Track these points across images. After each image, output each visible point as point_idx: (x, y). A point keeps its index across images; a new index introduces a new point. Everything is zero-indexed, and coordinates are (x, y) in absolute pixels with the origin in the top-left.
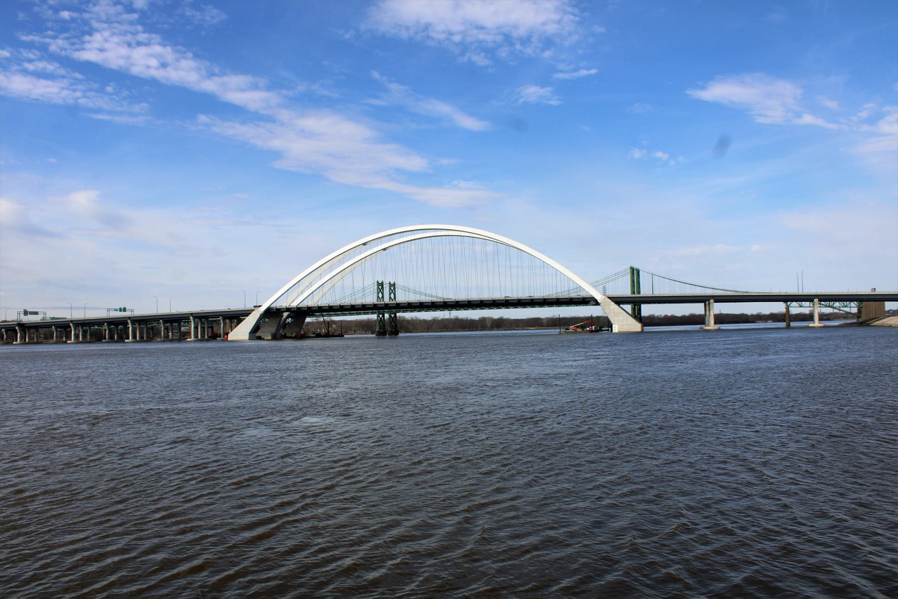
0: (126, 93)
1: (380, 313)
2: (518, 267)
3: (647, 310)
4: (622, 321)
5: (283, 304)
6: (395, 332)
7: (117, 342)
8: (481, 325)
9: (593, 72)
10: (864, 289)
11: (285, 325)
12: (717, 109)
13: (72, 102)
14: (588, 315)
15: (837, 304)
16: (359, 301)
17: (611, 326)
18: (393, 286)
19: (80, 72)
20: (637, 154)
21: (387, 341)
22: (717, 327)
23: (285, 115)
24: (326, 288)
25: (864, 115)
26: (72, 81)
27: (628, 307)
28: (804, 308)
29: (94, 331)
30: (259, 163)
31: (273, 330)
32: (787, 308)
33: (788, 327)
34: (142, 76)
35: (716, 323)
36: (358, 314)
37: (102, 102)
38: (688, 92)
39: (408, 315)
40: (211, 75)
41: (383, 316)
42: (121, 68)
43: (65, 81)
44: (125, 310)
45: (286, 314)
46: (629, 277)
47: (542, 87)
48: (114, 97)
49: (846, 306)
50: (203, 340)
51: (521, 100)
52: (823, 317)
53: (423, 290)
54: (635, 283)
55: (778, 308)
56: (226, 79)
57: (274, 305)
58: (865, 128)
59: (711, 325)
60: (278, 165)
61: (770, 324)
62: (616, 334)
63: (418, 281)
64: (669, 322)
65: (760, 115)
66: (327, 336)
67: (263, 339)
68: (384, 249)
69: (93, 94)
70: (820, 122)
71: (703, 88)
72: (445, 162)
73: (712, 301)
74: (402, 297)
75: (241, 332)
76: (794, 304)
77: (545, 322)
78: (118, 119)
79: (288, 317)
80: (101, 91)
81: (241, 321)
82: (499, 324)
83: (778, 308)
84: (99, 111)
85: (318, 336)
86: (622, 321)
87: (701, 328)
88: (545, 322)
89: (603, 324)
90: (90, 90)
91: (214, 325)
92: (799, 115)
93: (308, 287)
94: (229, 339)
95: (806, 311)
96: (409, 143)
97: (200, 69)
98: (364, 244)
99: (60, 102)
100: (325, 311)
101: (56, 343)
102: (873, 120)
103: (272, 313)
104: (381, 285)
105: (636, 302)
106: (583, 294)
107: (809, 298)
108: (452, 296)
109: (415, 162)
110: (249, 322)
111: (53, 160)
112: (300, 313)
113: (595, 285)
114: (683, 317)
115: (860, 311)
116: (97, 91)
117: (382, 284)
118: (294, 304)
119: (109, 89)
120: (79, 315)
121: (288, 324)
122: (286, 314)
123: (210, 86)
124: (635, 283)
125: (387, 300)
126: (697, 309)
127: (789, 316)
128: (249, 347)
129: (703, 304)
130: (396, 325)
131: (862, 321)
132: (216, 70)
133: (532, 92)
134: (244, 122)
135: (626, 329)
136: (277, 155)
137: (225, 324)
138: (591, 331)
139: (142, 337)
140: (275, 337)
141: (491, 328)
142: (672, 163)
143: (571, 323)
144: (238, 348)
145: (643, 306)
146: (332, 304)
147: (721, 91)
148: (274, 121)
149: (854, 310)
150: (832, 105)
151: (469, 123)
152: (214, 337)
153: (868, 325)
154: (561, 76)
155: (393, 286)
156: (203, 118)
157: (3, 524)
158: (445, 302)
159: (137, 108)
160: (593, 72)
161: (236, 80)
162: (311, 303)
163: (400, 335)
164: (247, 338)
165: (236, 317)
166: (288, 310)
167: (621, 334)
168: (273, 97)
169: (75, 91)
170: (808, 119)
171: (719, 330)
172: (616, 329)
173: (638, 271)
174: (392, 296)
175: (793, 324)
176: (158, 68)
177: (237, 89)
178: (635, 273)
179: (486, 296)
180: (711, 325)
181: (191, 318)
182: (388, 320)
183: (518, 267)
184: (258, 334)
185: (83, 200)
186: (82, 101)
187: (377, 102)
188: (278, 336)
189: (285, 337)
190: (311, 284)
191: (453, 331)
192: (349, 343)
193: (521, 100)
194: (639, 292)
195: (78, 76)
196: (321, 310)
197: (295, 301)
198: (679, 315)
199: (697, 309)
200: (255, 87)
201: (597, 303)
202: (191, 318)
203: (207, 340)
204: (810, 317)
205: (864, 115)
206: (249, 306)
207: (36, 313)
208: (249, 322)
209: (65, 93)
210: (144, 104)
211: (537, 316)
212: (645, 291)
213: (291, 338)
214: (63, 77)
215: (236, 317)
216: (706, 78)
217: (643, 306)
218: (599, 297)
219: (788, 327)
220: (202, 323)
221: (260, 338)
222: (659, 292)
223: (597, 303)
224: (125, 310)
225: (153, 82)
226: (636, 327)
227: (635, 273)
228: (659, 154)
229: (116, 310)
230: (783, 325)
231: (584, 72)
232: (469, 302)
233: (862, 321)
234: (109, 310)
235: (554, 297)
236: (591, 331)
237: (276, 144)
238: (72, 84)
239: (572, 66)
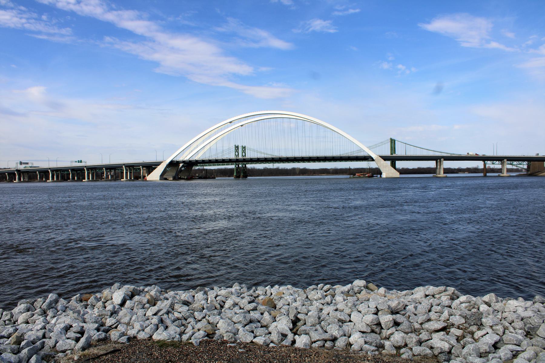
0: (54, 21)
2: (309, 137)
3: (400, 164)
4: (388, 171)
5: (181, 159)
6: (245, 176)
7: (76, 181)
8: (293, 172)
9: (358, 11)
10: (532, 154)
11: (181, 171)
12: (436, 35)
13: (20, 26)
15: (515, 163)
16: (226, 157)
18: (244, 148)
19: (24, 6)
20: (385, 66)
21: (241, 181)
22: (445, 175)
23: (162, 37)
24: (206, 149)
25: (530, 42)
26: (19, 11)
27: (389, 163)
28: (497, 165)
29: (62, 174)
30: (147, 70)
31: (174, 174)
32: (485, 165)
33: (485, 176)
34: (65, 9)
35: (444, 173)
36: (213, 165)
37: (40, 27)
38: (419, 25)
39: (249, 166)
40: (111, 9)
41: (238, 165)
42: (50, 3)
43: (14, 11)
44: (81, 162)
45: (181, 165)
46: (389, 144)
47: (325, 21)
48: (48, 23)
49: (520, 164)
50: (58, 180)
51: (311, 29)
52: (509, 170)
53: (263, 151)
54: (393, 149)
55: (480, 164)
56: (120, 12)
57: (175, 159)
58: (531, 51)
59: (442, 174)
60: (157, 71)
61: (467, 174)
63: (261, 145)
64: (429, 172)
65: (464, 42)
69: (33, 21)
70: (502, 47)
71: (429, 23)
72: (264, 69)
73: (442, 159)
74: (250, 155)
75: (155, 176)
76: (489, 162)
77: (331, 171)
78: (56, 39)
79: (183, 166)
80: (39, 20)
82: (304, 172)
83: (480, 164)
84: (39, 33)
86: (388, 171)
87: (434, 176)
88: (331, 171)
89: (378, 172)
90: (31, 18)
91: (138, 171)
92: (488, 42)
93: (195, 148)
95: (499, 166)
96: (244, 56)
97: (102, 5)
98: (230, 122)
99: (12, 26)
101: (40, 182)
102: (536, 46)
103: (173, 164)
104: (237, 147)
105: (393, 160)
106: (366, 155)
107: (500, 159)
108: (277, 154)
109: (245, 69)
110: (159, 170)
111: (14, 66)
112: (189, 164)
113: (370, 148)
114: (413, 169)
115: (529, 167)
116: (35, 19)
117: (238, 147)
119: (44, 17)
120: (54, 165)
121: (184, 171)
122: (181, 165)
123: (111, 17)
124: (393, 149)
125: (240, 157)
126: (432, 164)
127: (487, 170)
128: (160, 184)
129: (435, 162)
131: (531, 173)
132: (114, 6)
133: (318, 24)
134: (134, 42)
135: (390, 175)
136: (156, 64)
137: (126, 169)
138: (369, 177)
139: (131, 178)
140: (175, 179)
141: (299, 175)
142: (408, 72)
144: (154, 185)
147: (441, 25)
148: (154, 41)
149: (526, 167)
150: (510, 35)
151: (278, 44)
152: (137, 178)
153: (536, 176)
154: (336, 13)
155: (244, 148)
156: (108, 39)
158: (280, 158)
159: (64, 31)
160: (358, 11)
161: (127, 14)
162: (197, 158)
165: (150, 167)
166: (184, 162)
167: (387, 178)
168: (153, 26)
169: (21, 18)
170: (494, 45)
171: (446, 177)
172: (384, 175)
173: (395, 141)
174: (244, 154)
175: (488, 174)
176: (75, 4)
177: (129, 21)
178: (393, 142)
180: (505, 174)
181: (124, 166)
182: (240, 169)
183: (309, 137)
184: (165, 177)
185: (36, 92)
186: (27, 26)
187: (220, 29)
189: (181, 179)
190: (197, 147)
191: (261, 176)
192: (219, 182)
193: (311, 29)
195: (23, 8)
196: (204, 162)
197: (186, 157)
199: (432, 164)
200: (140, 18)
201: (373, 160)
202: (124, 166)
203: (133, 180)
204: (500, 171)
205: (530, 42)
207: (27, 163)
208: (159, 170)
209: (15, 20)
210: (68, 29)
212: (399, 152)
213: (184, 179)
214: (12, 9)
215: (150, 167)
216: (430, 17)
218: (374, 156)
219: (485, 176)
220: (130, 169)
221: (166, 179)
223: (373, 160)
224: (81, 162)
225: (72, 13)
226: (397, 175)
227: (393, 142)
228: (400, 66)
229: (76, 162)
230: (482, 174)
231: (352, 11)
232: (295, 158)
233: (531, 173)
234: (72, 162)
236: (369, 177)
237: (156, 57)
238: (19, 14)
239: (344, 7)
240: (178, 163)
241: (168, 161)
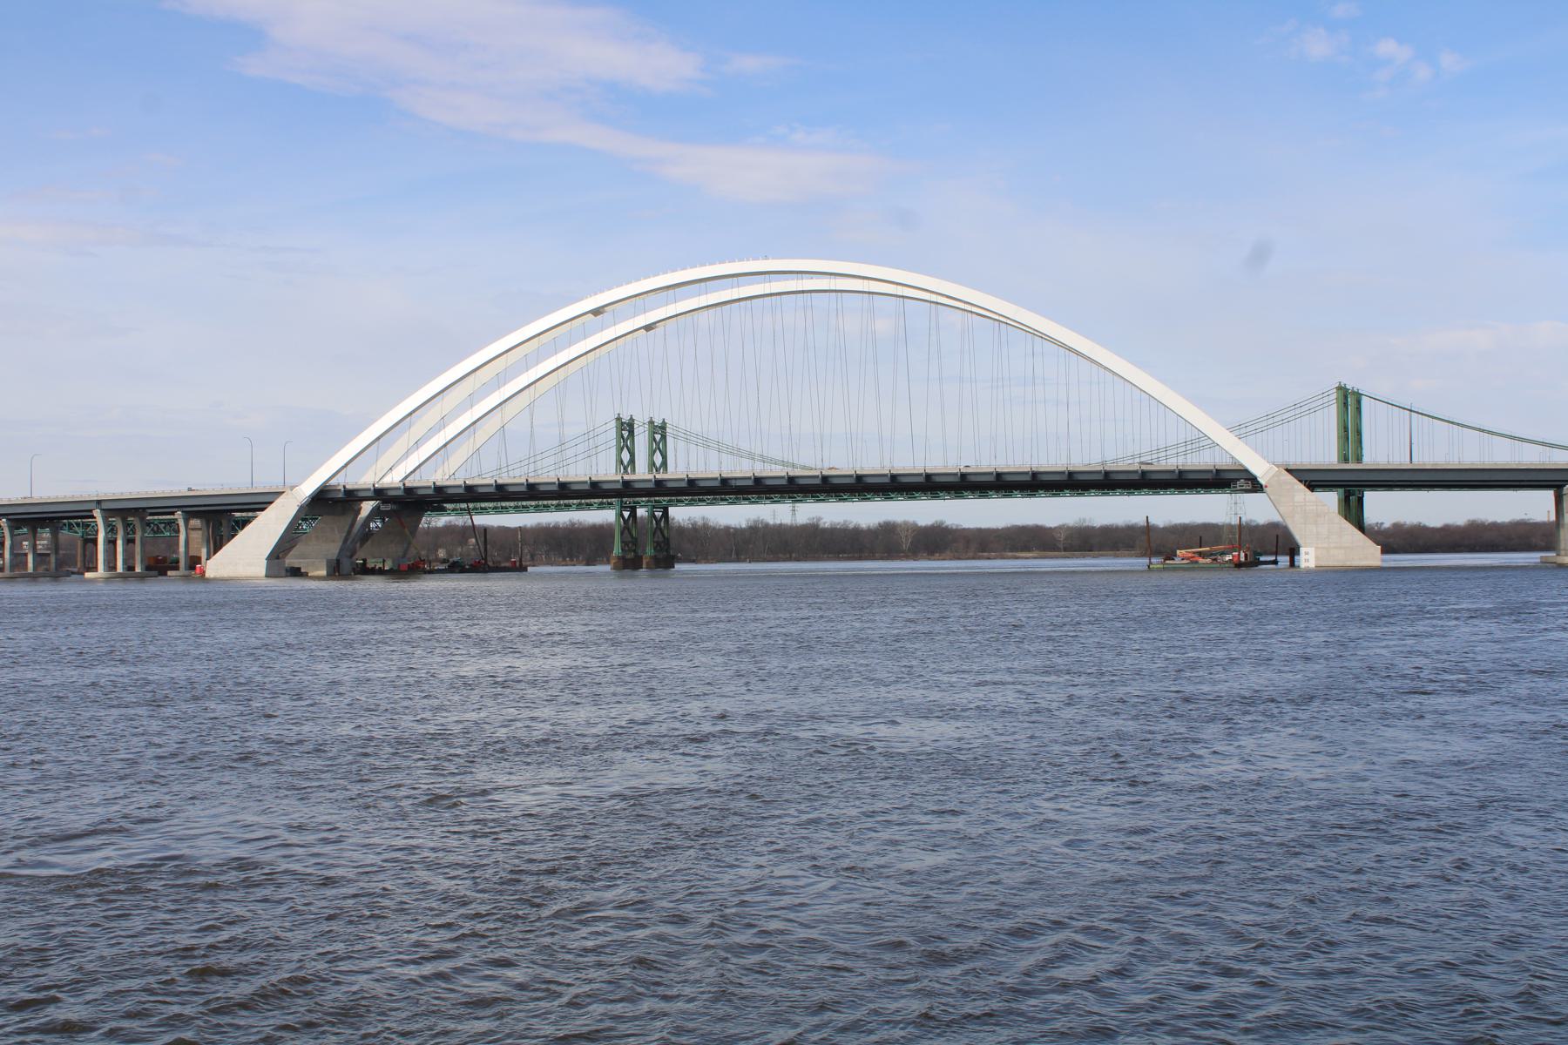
1: (623, 507)
3: (1382, 507)
4: (1325, 538)
5: (364, 478)
6: (665, 560)
8: (884, 543)
14: (1138, 519)
16: (578, 472)
17: (1293, 551)
18: (659, 432)
21: (643, 583)
24: (482, 434)
27: (1331, 499)
31: (333, 550)
45: (367, 507)
46: (1333, 411)
53: (745, 446)
57: (333, 482)
62: (1308, 571)
66: (480, 567)
67: (304, 575)
68: (648, 328)
74: (683, 464)
75: (244, 557)
79: (375, 513)
81: (244, 523)
82: (935, 541)
85: (455, 568)
86: (1325, 538)
87: (1544, 561)
91: (165, 535)
94: (209, 574)
98: (597, 312)
100: (486, 497)
103: (329, 503)
104: (626, 429)
105: (1350, 486)
106: (1222, 462)
109: (661, 64)
110: (266, 529)
112: (408, 504)
113: (1240, 430)
114: (1447, 530)
117: (663, 427)
118: (394, 479)
121: (383, 533)
122: (367, 507)
125: (642, 472)
129: (1549, 495)
130: (667, 541)
137: (111, 529)
143: (1177, 542)
144: (237, 601)
145: (1370, 498)
146: (504, 479)
152: (159, 566)
157: (1565, 924)
162: (448, 474)
163: (678, 566)
164: (263, 572)
165: (223, 518)
166: (379, 494)
172: (1308, 558)
173: (1358, 397)
174: (658, 459)
178: (1349, 401)
179: (873, 463)
181: (97, 513)
182: (641, 526)
188: (346, 565)
189: (365, 571)
190: (443, 423)
191: (872, 557)
194: (1359, 459)
196: (471, 496)
198: (1387, 525)
201: (1255, 486)
203: (141, 577)
206: (262, 484)
208: (266, 529)
211: (1040, 523)
212: (1379, 452)
215: (223, 518)
217: (1370, 498)
218: (1259, 468)
220: (127, 525)
221: (296, 572)
222: (1437, 453)
223: (1255, 486)
226: (1369, 554)
227: (1349, 401)
235: (1136, 467)
236: (1239, 565)
240: (351, 498)
241: (308, 488)
